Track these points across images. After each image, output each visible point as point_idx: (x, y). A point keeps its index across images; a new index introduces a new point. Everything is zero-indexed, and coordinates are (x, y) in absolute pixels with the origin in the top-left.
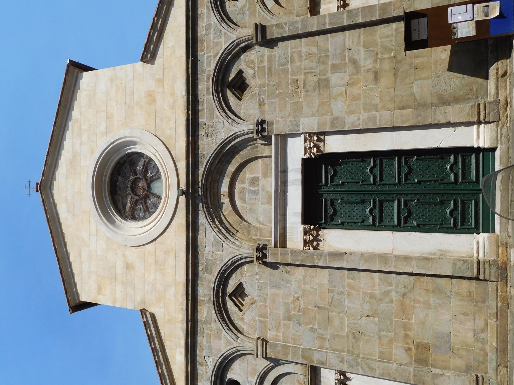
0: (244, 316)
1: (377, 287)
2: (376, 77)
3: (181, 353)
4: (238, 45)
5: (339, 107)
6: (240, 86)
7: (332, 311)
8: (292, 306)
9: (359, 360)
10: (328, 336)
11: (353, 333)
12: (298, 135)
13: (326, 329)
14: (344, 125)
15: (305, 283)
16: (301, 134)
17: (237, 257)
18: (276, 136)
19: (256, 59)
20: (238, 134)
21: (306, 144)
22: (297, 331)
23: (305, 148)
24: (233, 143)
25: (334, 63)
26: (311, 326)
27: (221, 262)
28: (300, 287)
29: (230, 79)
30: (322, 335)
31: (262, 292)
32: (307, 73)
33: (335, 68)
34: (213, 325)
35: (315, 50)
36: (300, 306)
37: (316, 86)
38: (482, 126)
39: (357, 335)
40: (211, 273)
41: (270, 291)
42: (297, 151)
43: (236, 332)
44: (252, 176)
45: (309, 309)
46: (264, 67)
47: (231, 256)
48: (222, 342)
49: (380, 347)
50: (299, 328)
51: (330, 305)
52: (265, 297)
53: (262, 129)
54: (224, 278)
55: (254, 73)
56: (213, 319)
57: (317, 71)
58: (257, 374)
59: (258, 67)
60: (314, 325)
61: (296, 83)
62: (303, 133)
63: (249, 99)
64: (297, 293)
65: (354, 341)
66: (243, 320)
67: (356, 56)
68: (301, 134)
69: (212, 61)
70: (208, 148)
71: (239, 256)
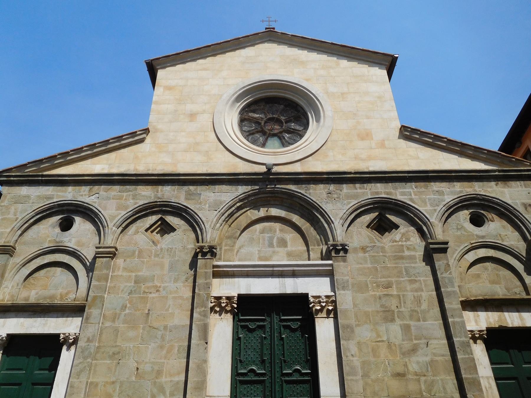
0: (140, 233)
1: (169, 379)
2: (400, 375)
3: (103, 169)
4: (425, 224)
5: (365, 333)
6: (382, 226)
7: (144, 329)
8: (151, 284)
9: (89, 360)
10: (116, 324)
11: (119, 353)
12: (333, 289)
13: (125, 322)
14: (345, 340)
15: (175, 298)
16: (335, 292)
17: (203, 225)
18: (331, 265)
20: (332, 225)
22: (123, 290)
23: (319, 297)
26: (128, 305)
28: (171, 293)
29: (388, 216)
30: (118, 318)
31: (166, 253)
33: (406, 329)
34: (132, 201)
35: (424, 306)
36: (151, 293)
39: (116, 356)
41: (167, 262)
42: (316, 288)
44: (288, 240)
45: (147, 303)
46: (403, 252)
47: (204, 219)
48: (114, 211)
49: (103, 383)
50: (126, 292)
51: (150, 326)
52: (161, 256)
53: (338, 250)
54: (181, 212)
55: (396, 241)
57: (403, 309)
58: (78, 249)
59: (403, 246)
60: (129, 309)
61: (388, 286)
62: (335, 294)
63: (368, 236)
64: (164, 290)
65: (111, 353)
66: (137, 232)
67: (420, 352)
68: (335, 292)
69: (406, 197)
70: (317, 194)
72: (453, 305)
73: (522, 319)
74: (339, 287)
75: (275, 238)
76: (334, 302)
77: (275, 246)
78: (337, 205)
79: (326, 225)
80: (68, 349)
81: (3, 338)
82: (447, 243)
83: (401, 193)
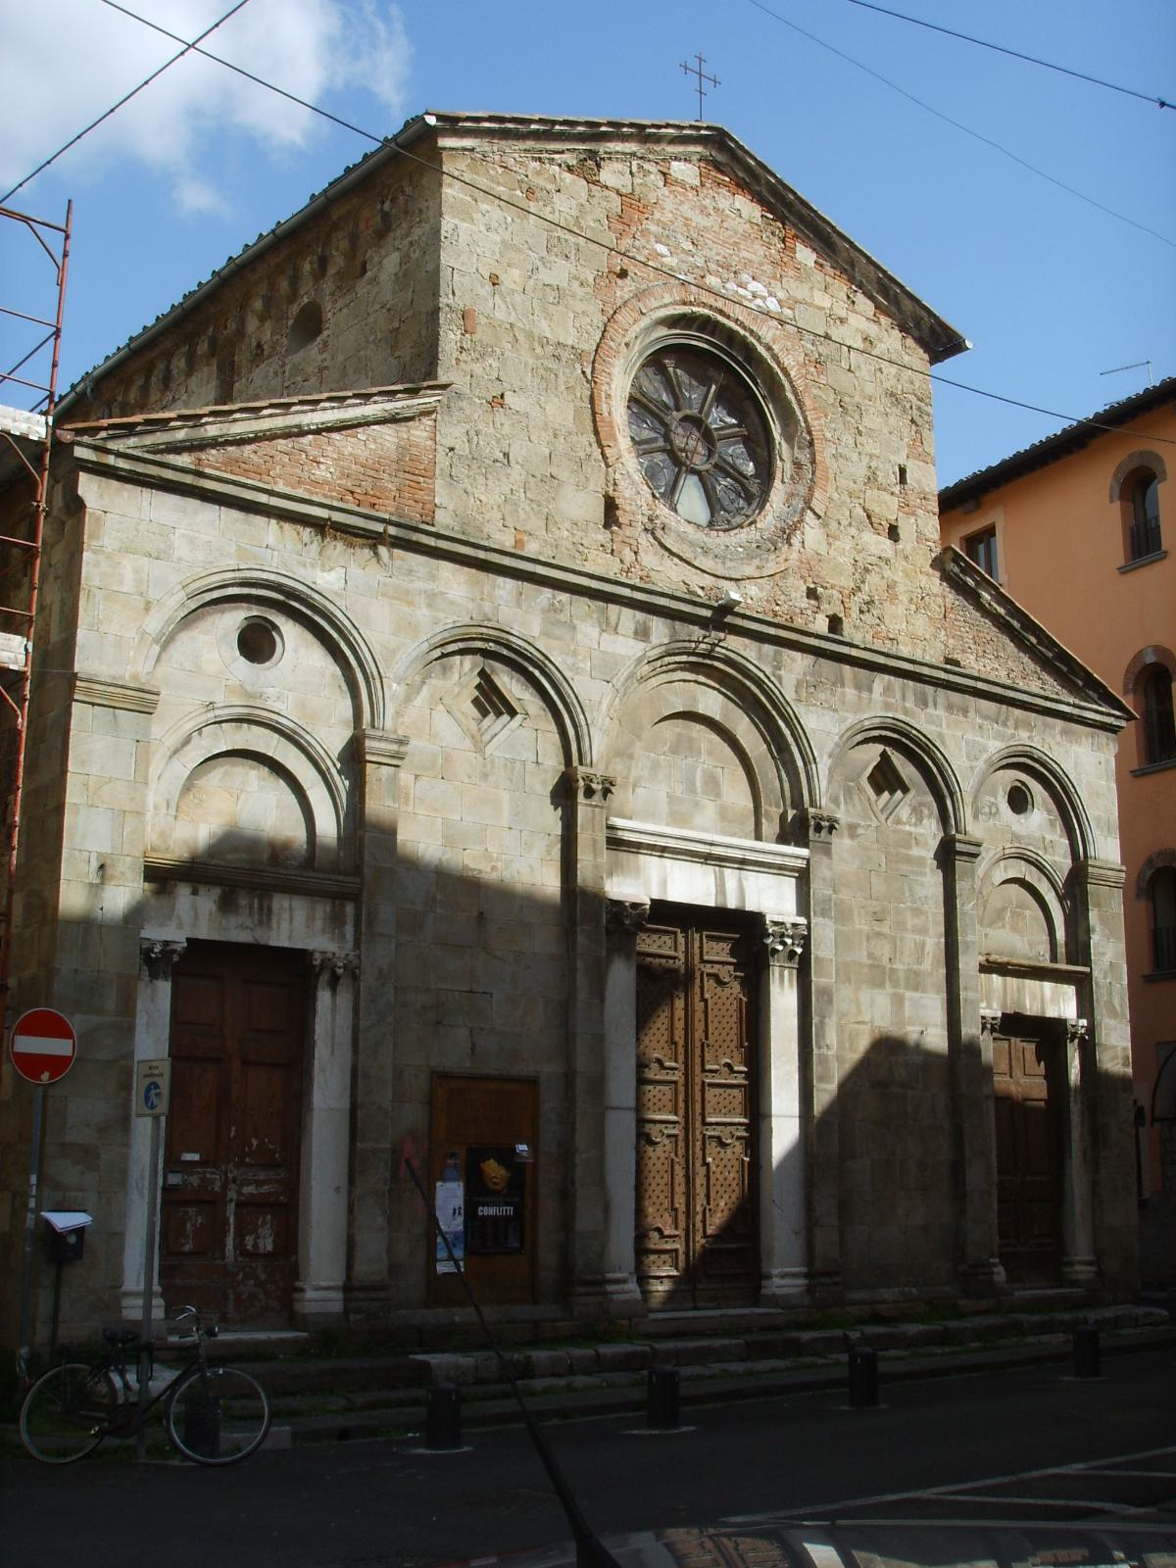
4: (952, 794)
6: (491, 701)
12: (804, 906)
16: (808, 917)
17: (581, 717)
19: (922, 831)
20: (814, 766)
21: (788, 926)
24: (794, 749)
27: (571, 670)
32: (895, 942)
34: (425, 611)
37: (875, 959)
38: (339, 1295)
40: (546, 634)
42: (771, 898)
43: (216, 594)
46: (910, 847)
54: (525, 664)
56: (441, 615)
57: (898, 966)
59: (910, 834)
68: (808, 917)
71: (583, 723)
72: (968, 964)
73: (721, 889)
74: (817, 909)
75: (699, 769)
76: (806, 941)
77: (699, 790)
78: (830, 718)
79: (800, 763)
80: (334, 983)
81: (174, 951)
82: (979, 845)
83: (333, 575)
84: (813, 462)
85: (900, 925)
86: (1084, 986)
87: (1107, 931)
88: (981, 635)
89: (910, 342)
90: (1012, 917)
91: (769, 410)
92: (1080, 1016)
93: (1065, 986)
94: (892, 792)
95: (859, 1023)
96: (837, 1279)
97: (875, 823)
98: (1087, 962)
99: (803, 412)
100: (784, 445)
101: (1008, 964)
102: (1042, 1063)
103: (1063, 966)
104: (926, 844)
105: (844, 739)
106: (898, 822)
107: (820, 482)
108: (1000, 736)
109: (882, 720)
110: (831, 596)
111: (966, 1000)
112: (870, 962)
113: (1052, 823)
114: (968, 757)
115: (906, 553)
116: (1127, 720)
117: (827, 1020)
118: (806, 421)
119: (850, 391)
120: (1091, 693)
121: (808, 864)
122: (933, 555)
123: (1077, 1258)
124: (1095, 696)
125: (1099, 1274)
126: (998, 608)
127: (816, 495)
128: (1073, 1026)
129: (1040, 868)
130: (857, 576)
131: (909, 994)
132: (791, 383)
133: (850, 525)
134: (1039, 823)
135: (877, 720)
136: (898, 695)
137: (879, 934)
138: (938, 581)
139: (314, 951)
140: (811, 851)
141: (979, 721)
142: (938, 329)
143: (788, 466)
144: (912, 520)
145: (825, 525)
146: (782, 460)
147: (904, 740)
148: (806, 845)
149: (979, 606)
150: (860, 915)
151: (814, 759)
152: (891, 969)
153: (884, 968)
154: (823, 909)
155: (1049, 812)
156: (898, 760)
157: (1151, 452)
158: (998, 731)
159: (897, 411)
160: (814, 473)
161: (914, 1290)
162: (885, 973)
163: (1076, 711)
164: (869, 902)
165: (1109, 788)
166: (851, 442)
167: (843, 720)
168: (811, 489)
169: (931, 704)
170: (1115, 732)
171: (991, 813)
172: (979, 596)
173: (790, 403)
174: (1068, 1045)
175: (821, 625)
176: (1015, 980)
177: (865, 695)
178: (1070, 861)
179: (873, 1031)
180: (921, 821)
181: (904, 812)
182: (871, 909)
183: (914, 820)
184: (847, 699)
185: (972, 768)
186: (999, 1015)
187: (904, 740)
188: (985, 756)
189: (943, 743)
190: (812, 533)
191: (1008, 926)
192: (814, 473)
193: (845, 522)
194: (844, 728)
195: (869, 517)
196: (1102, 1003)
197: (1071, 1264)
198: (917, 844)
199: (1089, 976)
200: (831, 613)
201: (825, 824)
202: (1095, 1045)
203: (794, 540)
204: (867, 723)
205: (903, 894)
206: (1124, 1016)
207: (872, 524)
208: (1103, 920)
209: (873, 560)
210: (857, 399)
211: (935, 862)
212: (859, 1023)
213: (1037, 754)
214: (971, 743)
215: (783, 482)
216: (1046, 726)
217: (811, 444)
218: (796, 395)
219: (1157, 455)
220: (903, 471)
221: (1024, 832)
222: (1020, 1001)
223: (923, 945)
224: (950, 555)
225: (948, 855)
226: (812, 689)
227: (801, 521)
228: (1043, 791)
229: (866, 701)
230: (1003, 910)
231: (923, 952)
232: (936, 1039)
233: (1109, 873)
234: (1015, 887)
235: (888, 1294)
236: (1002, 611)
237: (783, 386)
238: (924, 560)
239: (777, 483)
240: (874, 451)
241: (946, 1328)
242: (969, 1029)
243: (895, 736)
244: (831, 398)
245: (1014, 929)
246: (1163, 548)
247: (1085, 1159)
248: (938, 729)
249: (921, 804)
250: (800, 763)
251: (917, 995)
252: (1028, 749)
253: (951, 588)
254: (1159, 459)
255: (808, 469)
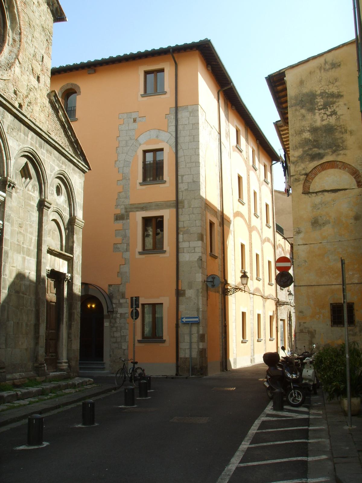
19: (34, 195)
25: (26, 261)
46: (31, 201)
57: (25, 246)
59: (31, 195)
62: (3, 224)
72: (44, 249)
74: (6, 218)
79: (5, 158)
84: (20, 41)
85: (26, 230)
86: (70, 261)
87: (78, 243)
88: (57, 127)
89: (49, 10)
90: (52, 233)
91: (7, 14)
92: (68, 272)
93: (65, 261)
94: (26, 178)
95: (13, 267)
96: (4, 370)
97: (22, 189)
98: (72, 253)
99: (19, 20)
100: (10, 31)
101: (54, 250)
102: (55, 289)
103: (63, 252)
104: (35, 200)
105: (19, 153)
106: (28, 190)
107: (22, 50)
108: (58, 166)
109: (31, 150)
110: (20, 96)
111: (43, 262)
112: (17, 243)
113: (66, 201)
114: (50, 171)
115: (42, 88)
116: (89, 170)
117: (6, 264)
118: (20, 24)
119: (32, 20)
120: (81, 157)
121: (5, 200)
122: (48, 92)
123: (63, 361)
124: (82, 159)
125: (69, 366)
126: (63, 118)
127: (20, 54)
128: (67, 276)
129: (61, 217)
130: (28, 91)
131: (27, 258)
132: (17, 7)
133: (27, 70)
134: (62, 200)
135: (28, 149)
136: (35, 141)
137: (20, 232)
138: (48, 103)
139: (288, 127)
140: (6, 195)
141: (54, 158)
142: (59, 9)
143: (11, 40)
144: (44, 77)
145: (21, 67)
146: (9, 36)
147: (34, 159)
148: (5, 192)
149: (58, 116)
150: (16, 224)
151: (10, 158)
152: (23, 247)
153: (21, 246)
154: (8, 219)
155: (65, 197)
156: (30, 166)
157: (76, 85)
158: (58, 163)
159: (43, 34)
160: (20, 45)
161: (23, 374)
162: (21, 248)
163: (77, 163)
164: (19, 219)
165: (82, 192)
166: (31, 39)
167: (19, 146)
168: (18, 51)
169: (43, 147)
170: (84, 173)
171: (52, 193)
172: (59, 112)
173: (15, 15)
174: (65, 283)
175: (17, 105)
176: (53, 256)
177: (26, 137)
178: (69, 216)
179: (17, 270)
180: (34, 191)
181: (30, 186)
182: (19, 222)
183: (32, 190)
184: (21, 137)
185: (51, 175)
186: (50, 270)
187: (34, 159)
188: (54, 172)
189: (45, 163)
190: (17, 69)
191: (51, 237)
192: (20, 45)
193: (26, 69)
194: (20, 149)
195: (32, 70)
196: (75, 269)
197: (61, 363)
198: (33, 200)
199: (72, 258)
200: (19, 102)
201: (12, 185)
202: (72, 284)
203: (12, 69)
204: (25, 149)
205: (28, 218)
206: (80, 274)
207: (33, 73)
208: (77, 238)
209: (33, 87)
210: (34, 24)
211: (37, 208)
212: (13, 267)
213: (66, 175)
214: (52, 164)
215: (8, 45)
216: (69, 165)
217: (20, 34)
218: (18, 12)
219: (78, 86)
220: (43, 57)
221: (59, 203)
222: (54, 265)
223: (32, 239)
224: (53, 94)
225: (42, 205)
226: (12, 130)
227: (14, 62)
228: (65, 189)
229: (26, 140)
230: (50, 230)
231: (31, 242)
232: (33, 276)
233: (80, 222)
234: (53, 222)
235: (17, 375)
236: (64, 120)
237: (14, 6)
238: (45, 93)
239: (6, 44)
240: (36, 46)
241: (43, 389)
242: (44, 274)
243: (31, 156)
244: (27, 19)
245: (53, 239)
246: (76, 117)
247: (66, 325)
248: (44, 158)
249: (35, 185)
250: (5, 158)
251: (29, 258)
252: (64, 172)
253: (51, 106)
254: (79, 87)
255: (18, 42)
